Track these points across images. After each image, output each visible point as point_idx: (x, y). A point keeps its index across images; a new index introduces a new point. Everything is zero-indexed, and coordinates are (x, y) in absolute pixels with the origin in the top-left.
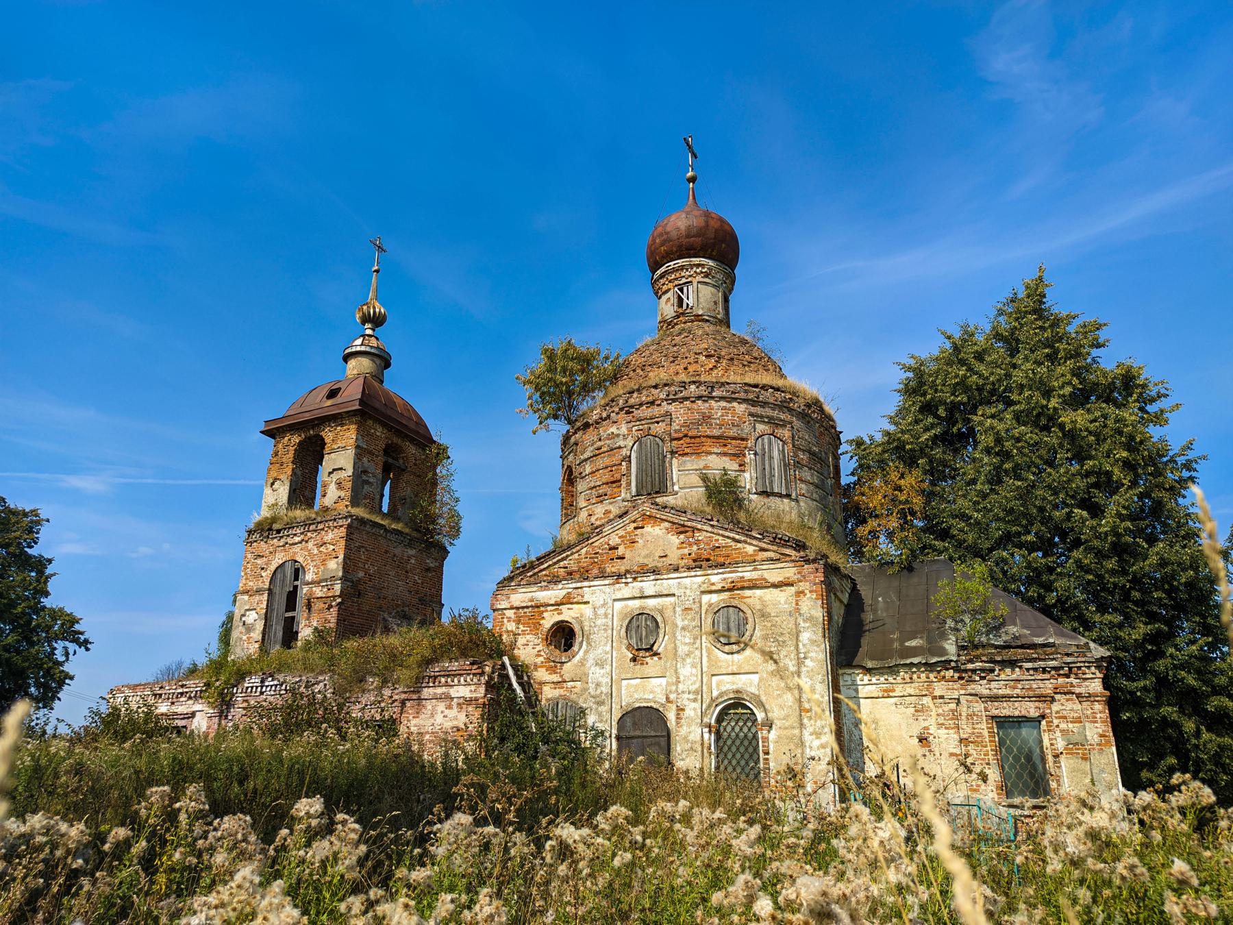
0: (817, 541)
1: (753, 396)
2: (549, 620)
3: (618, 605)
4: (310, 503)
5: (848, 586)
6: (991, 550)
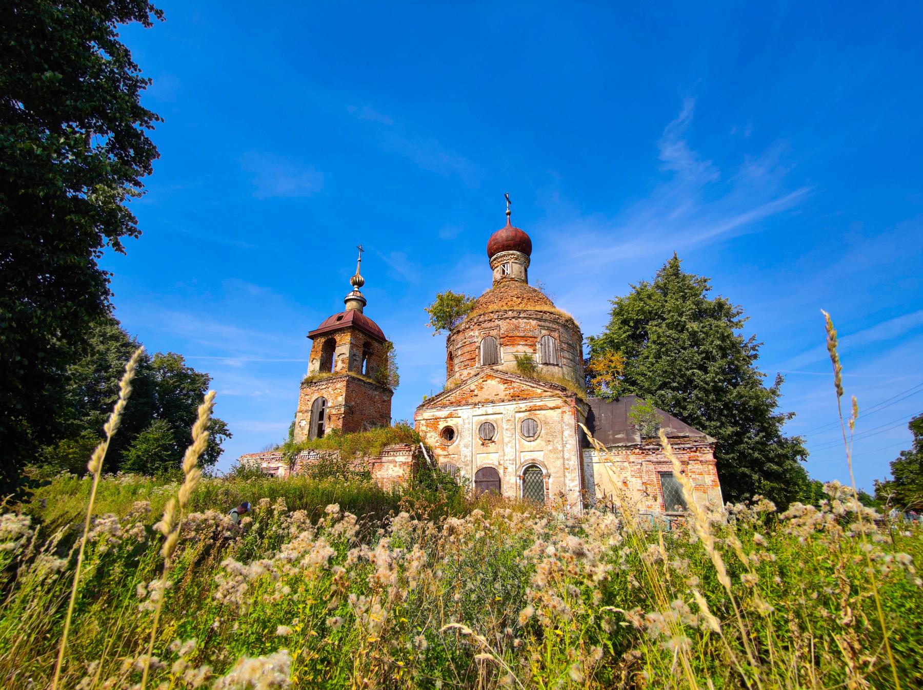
0: (572, 388)
1: (540, 317)
2: (442, 425)
3: (475, 419)
4: (329, 370)
5: (587, 408)
6: (656, 391)
